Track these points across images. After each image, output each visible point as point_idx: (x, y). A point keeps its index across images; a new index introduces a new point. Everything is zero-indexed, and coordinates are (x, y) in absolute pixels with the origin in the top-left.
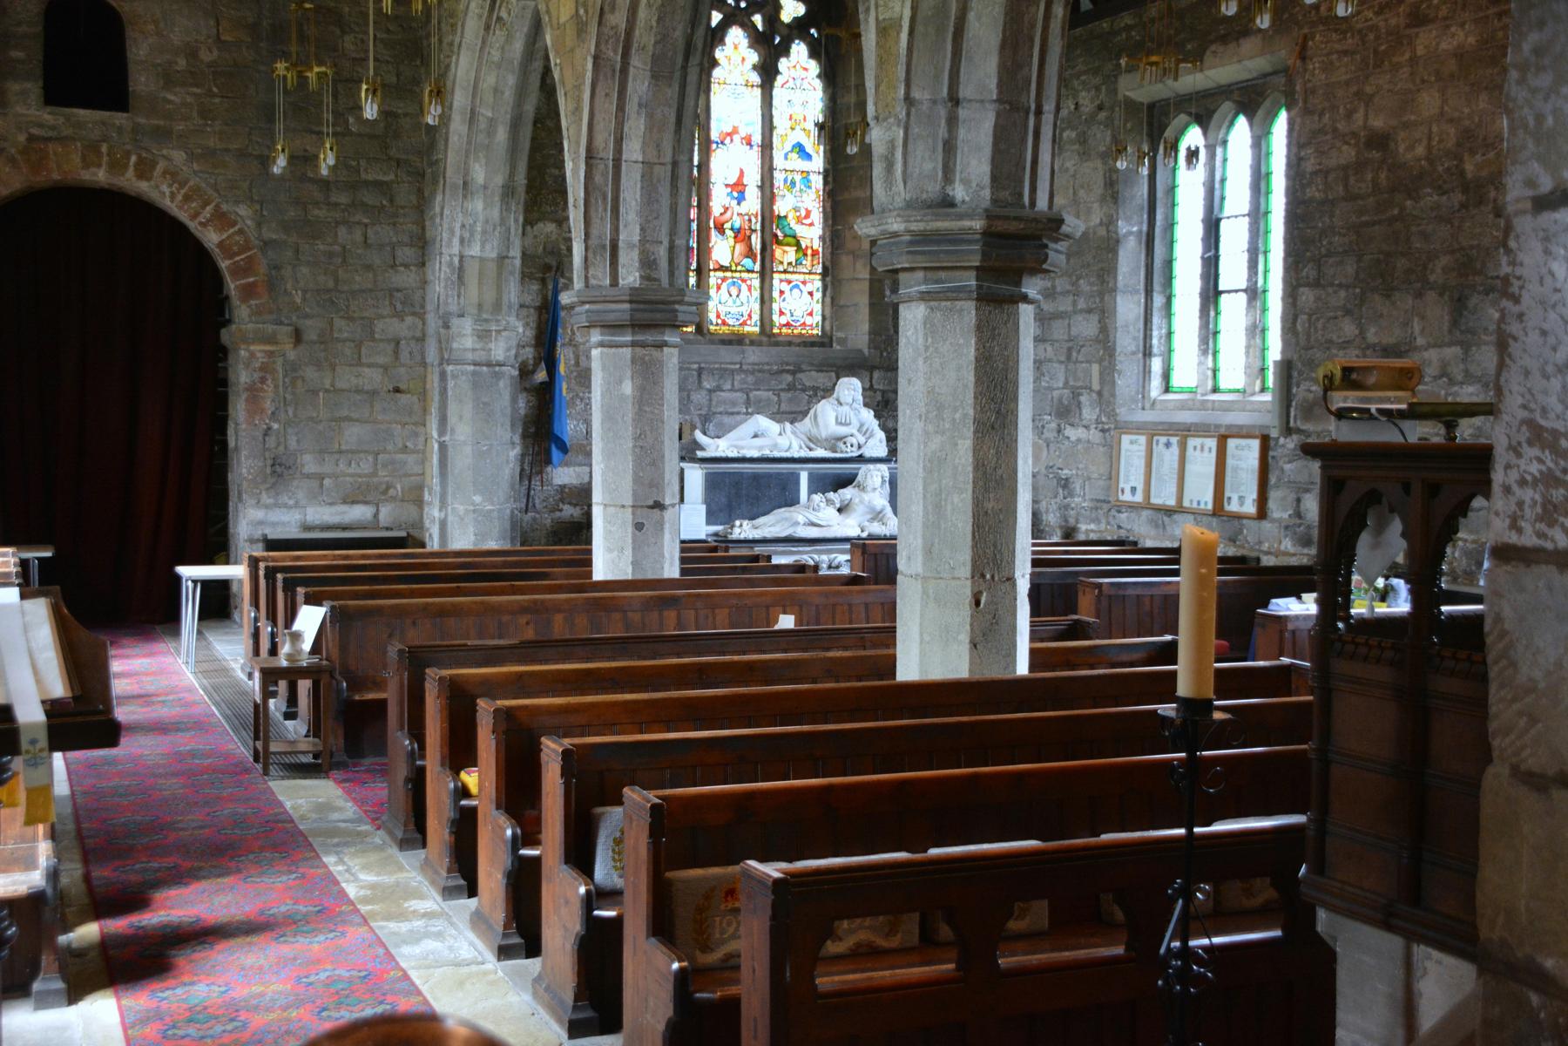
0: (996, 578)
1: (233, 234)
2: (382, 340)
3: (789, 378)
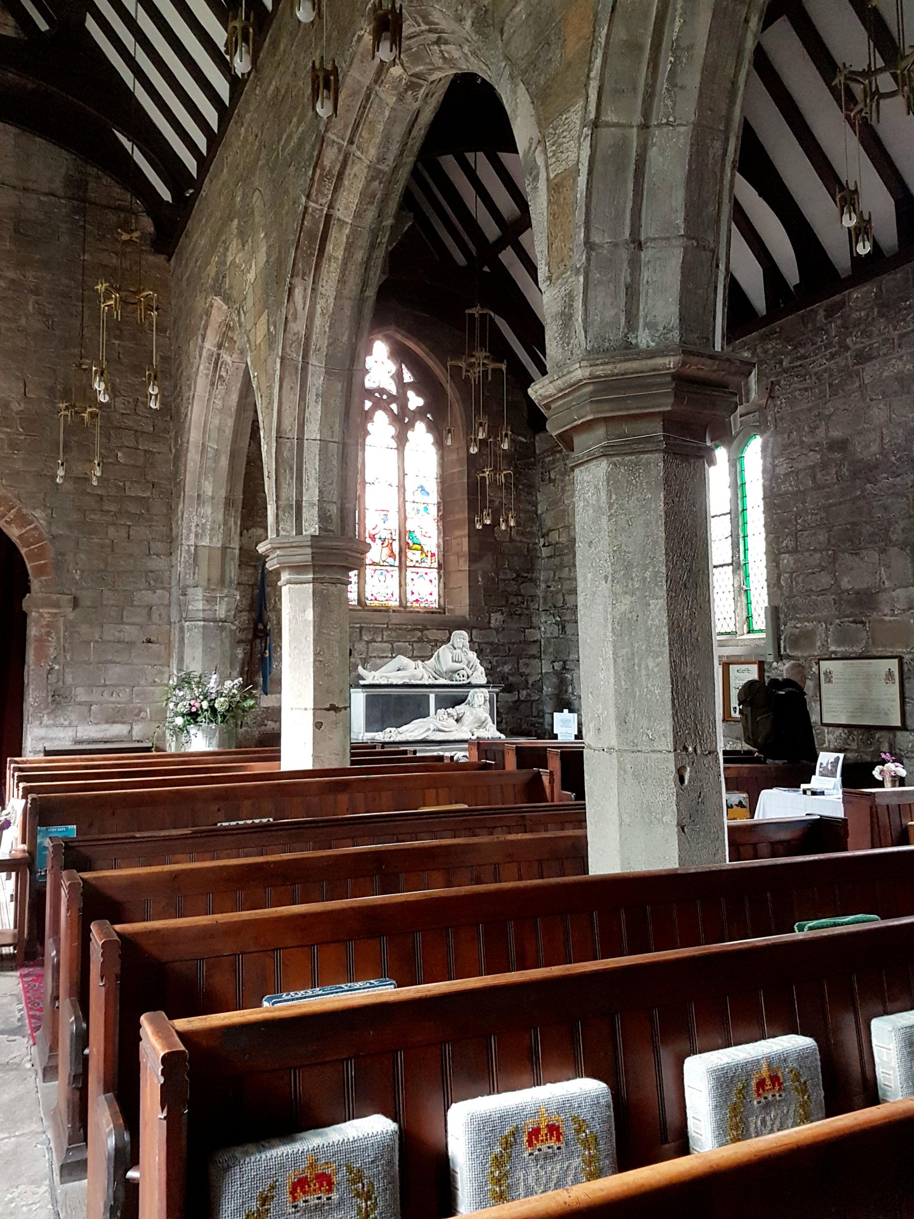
0: (699, 752)
1: (31, 529)
3: (420, 634)
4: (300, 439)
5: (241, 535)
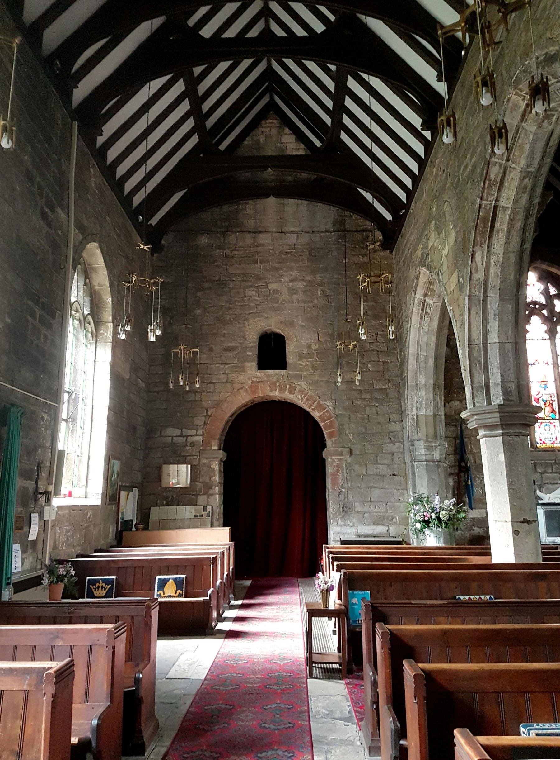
2: (386, 453)
4: (485, 344)
5: (445, 406)
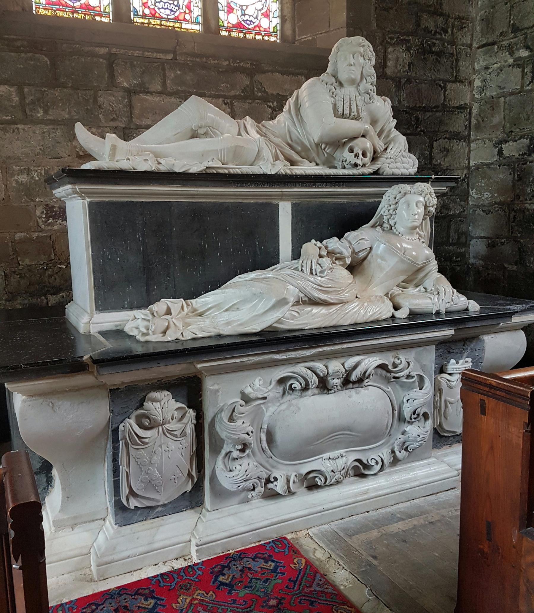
3: (246, 81)
